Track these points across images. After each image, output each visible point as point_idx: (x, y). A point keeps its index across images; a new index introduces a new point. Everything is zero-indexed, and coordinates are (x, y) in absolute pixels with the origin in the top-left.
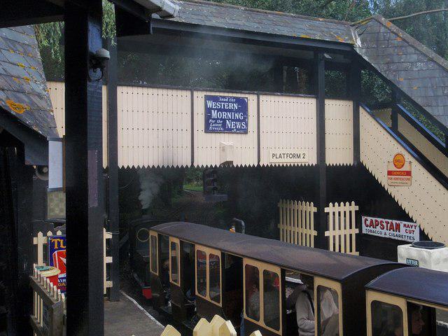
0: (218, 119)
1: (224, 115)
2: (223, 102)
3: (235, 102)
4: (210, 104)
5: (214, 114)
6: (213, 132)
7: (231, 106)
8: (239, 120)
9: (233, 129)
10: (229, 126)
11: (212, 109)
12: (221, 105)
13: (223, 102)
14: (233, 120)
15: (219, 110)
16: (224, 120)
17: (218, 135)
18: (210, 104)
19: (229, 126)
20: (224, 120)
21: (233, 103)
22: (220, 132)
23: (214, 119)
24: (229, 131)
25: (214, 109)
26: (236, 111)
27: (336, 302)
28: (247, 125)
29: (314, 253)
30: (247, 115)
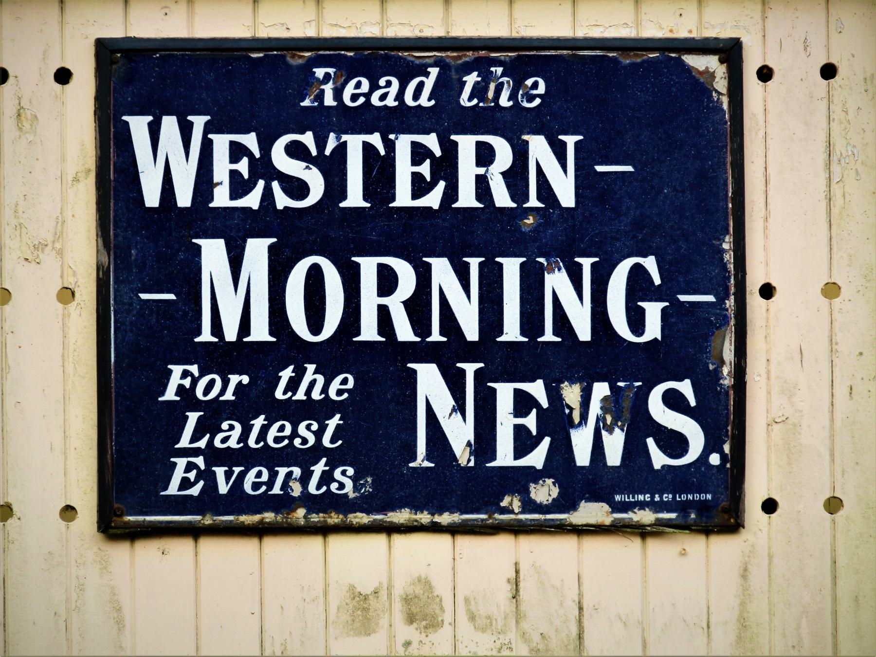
0: (286, 347)
1: (379, 298)
2: (362, 119)
3: (548, 123)
4: (166, 159)
5: (234, 289)
6: (222, 515)
7: (479, 172)
8: (605, 355)
9: (519, 480)
10: (460, 433)
11: (203, 218)
12: (334, 168)
13: (362, 119)
14: (504, 362)
15: (293, 236)
16: (383, 370)
17: (95, 272)
18: (166, 159)
19: (460, 433)
20: (383, 370)
21: (514, 125)
22: (327, 518)
23: (222, 357)
24: (471, 496)
25: (235, 230)
26: (558, 237)
27: (564, 167)
28: (724, 414)
29: (685, 27)
30: (729, 280)
